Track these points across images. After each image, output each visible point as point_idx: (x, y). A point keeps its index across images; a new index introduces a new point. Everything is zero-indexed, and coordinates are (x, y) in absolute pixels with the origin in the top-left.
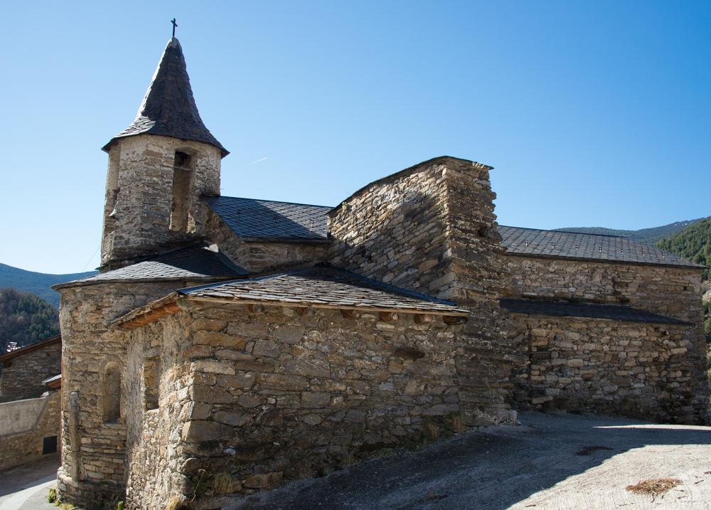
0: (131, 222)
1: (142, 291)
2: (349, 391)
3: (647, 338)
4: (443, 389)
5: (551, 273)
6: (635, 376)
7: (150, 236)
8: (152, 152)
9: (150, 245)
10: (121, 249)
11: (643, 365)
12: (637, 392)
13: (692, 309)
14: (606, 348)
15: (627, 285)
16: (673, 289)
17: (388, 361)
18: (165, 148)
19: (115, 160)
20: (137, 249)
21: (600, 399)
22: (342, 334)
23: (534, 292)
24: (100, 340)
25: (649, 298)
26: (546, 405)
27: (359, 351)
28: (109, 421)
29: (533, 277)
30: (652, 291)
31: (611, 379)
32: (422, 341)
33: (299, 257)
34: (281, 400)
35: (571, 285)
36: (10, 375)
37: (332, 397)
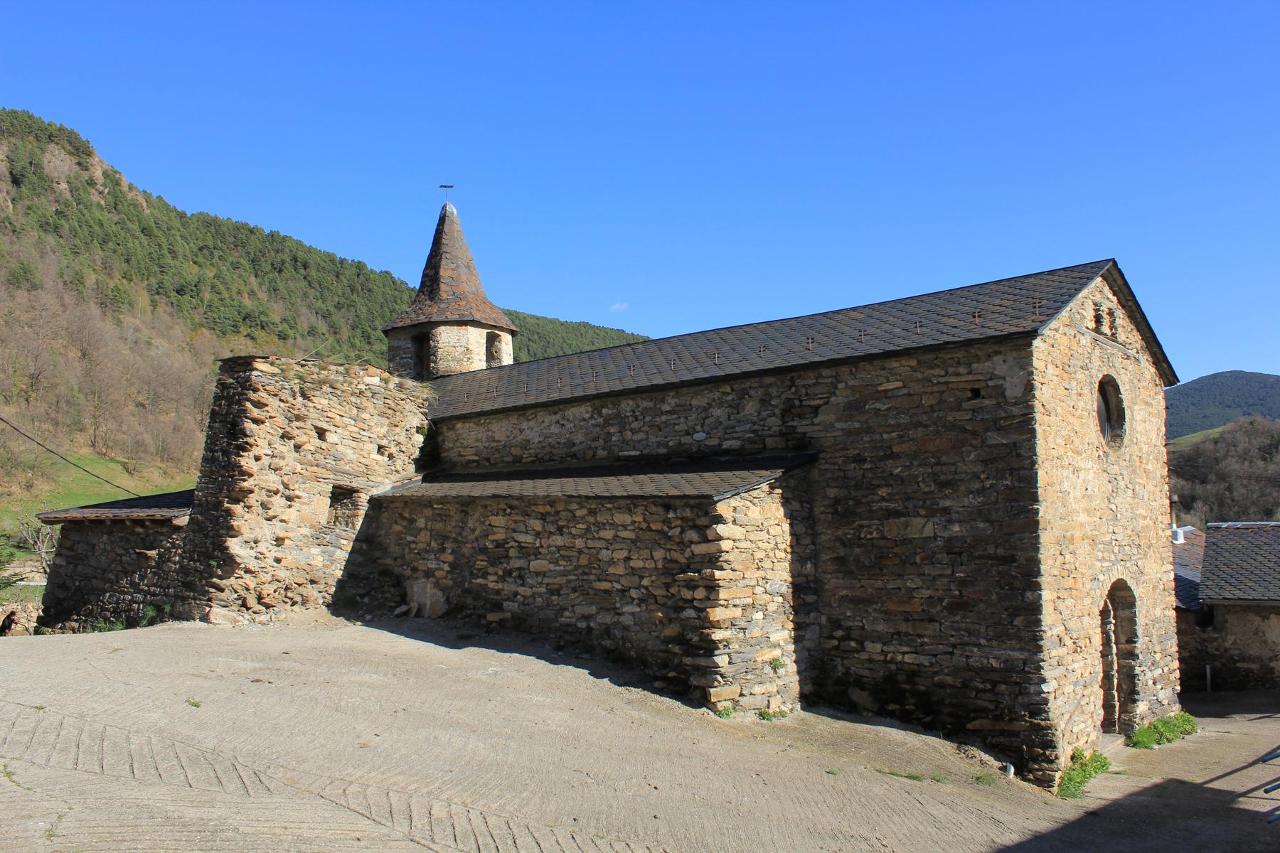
3: (644, 525)
5: (668, 412)
6: (623, 592)
12: (627, 620)
14: (579, 543)
15: (816, 410)
23: (634, 449)
25: (868, 430)
26: (502, 622)
29: (635, 425)
35: (698, 428)
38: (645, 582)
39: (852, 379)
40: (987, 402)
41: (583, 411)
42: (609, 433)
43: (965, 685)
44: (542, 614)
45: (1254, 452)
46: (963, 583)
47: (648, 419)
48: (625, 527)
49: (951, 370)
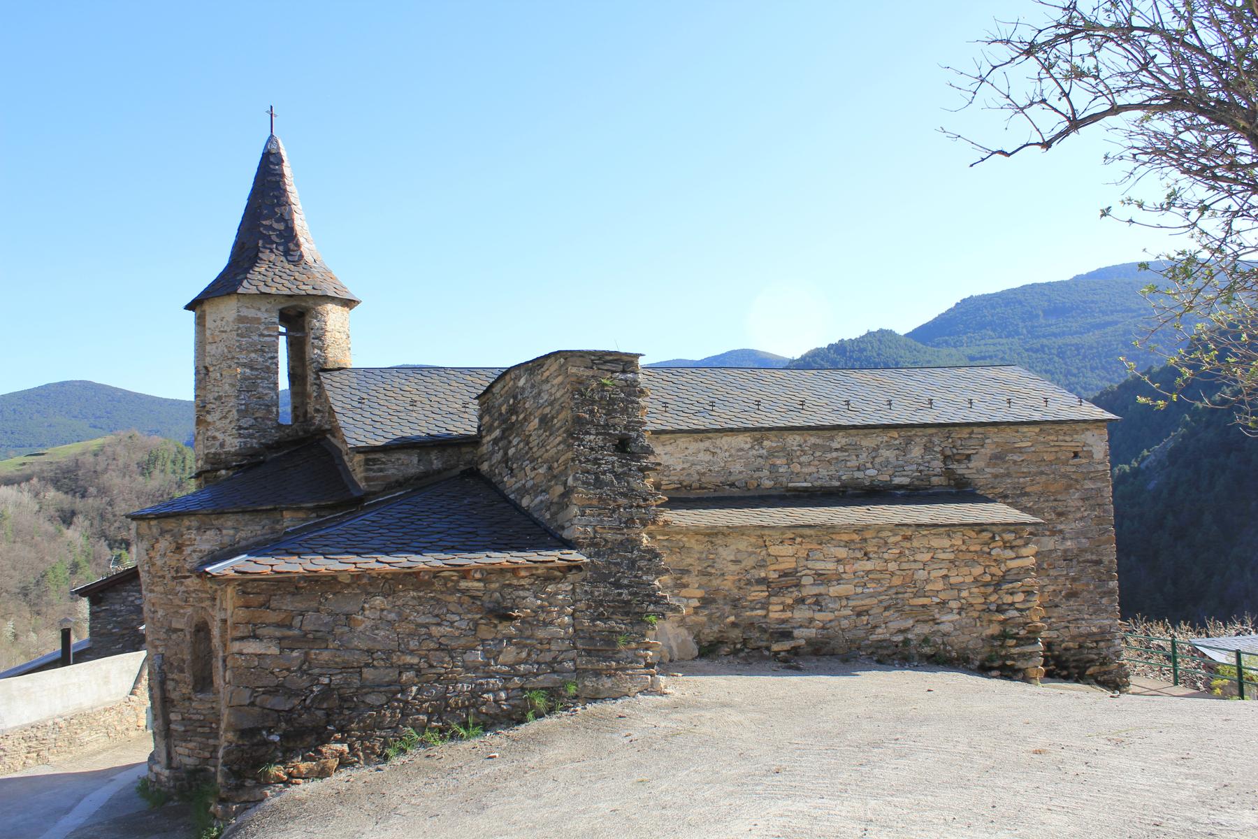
0: (225, 417)
1: (230, 523)
2: (423, 665)
3: (964, 548)
4: (553, 654)
5: (836, 450)
6: (943, 603)
7: (251, 436)
8: (246, 317)
9: (251, 447)
10: (215, 454)
11: (958, 588)
12: (946, 628)
13: (1089, 485)
14: (892, 566)
15: (968, 457)
16: (1052, 457)
17: (476, 624)
18: (263, 309)
19: (200, 322)
20: (236, 454)
21: (884, 640)
22: (413, 598)
24: (183, 588)
25: (1008, 475)
26: (795, 651)
27: (437, 616)
28: (202, 691)
30: (1015, 462)
31: (900, 611)
32: (524, 598)
33: (437, 464)
34: (337, 679)
35: (869, 465)
36: (102, 614)
37: (400, 673)
38: (964, 594)
39: (995, 437)
40: (1084, 461)
41: (742, 441)
42: (774, 465)
43: (1081, 647)
44: (848, 635)
45: (134, 467)
46: (1074, 580)
47: (818, 454)
48: (944, 550)
49: (1061, 438)
